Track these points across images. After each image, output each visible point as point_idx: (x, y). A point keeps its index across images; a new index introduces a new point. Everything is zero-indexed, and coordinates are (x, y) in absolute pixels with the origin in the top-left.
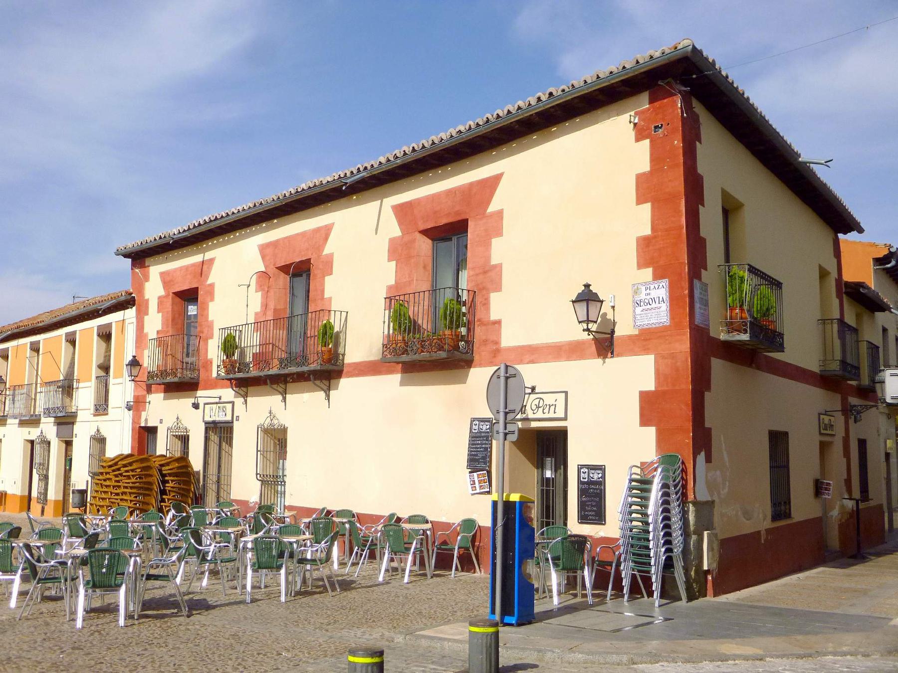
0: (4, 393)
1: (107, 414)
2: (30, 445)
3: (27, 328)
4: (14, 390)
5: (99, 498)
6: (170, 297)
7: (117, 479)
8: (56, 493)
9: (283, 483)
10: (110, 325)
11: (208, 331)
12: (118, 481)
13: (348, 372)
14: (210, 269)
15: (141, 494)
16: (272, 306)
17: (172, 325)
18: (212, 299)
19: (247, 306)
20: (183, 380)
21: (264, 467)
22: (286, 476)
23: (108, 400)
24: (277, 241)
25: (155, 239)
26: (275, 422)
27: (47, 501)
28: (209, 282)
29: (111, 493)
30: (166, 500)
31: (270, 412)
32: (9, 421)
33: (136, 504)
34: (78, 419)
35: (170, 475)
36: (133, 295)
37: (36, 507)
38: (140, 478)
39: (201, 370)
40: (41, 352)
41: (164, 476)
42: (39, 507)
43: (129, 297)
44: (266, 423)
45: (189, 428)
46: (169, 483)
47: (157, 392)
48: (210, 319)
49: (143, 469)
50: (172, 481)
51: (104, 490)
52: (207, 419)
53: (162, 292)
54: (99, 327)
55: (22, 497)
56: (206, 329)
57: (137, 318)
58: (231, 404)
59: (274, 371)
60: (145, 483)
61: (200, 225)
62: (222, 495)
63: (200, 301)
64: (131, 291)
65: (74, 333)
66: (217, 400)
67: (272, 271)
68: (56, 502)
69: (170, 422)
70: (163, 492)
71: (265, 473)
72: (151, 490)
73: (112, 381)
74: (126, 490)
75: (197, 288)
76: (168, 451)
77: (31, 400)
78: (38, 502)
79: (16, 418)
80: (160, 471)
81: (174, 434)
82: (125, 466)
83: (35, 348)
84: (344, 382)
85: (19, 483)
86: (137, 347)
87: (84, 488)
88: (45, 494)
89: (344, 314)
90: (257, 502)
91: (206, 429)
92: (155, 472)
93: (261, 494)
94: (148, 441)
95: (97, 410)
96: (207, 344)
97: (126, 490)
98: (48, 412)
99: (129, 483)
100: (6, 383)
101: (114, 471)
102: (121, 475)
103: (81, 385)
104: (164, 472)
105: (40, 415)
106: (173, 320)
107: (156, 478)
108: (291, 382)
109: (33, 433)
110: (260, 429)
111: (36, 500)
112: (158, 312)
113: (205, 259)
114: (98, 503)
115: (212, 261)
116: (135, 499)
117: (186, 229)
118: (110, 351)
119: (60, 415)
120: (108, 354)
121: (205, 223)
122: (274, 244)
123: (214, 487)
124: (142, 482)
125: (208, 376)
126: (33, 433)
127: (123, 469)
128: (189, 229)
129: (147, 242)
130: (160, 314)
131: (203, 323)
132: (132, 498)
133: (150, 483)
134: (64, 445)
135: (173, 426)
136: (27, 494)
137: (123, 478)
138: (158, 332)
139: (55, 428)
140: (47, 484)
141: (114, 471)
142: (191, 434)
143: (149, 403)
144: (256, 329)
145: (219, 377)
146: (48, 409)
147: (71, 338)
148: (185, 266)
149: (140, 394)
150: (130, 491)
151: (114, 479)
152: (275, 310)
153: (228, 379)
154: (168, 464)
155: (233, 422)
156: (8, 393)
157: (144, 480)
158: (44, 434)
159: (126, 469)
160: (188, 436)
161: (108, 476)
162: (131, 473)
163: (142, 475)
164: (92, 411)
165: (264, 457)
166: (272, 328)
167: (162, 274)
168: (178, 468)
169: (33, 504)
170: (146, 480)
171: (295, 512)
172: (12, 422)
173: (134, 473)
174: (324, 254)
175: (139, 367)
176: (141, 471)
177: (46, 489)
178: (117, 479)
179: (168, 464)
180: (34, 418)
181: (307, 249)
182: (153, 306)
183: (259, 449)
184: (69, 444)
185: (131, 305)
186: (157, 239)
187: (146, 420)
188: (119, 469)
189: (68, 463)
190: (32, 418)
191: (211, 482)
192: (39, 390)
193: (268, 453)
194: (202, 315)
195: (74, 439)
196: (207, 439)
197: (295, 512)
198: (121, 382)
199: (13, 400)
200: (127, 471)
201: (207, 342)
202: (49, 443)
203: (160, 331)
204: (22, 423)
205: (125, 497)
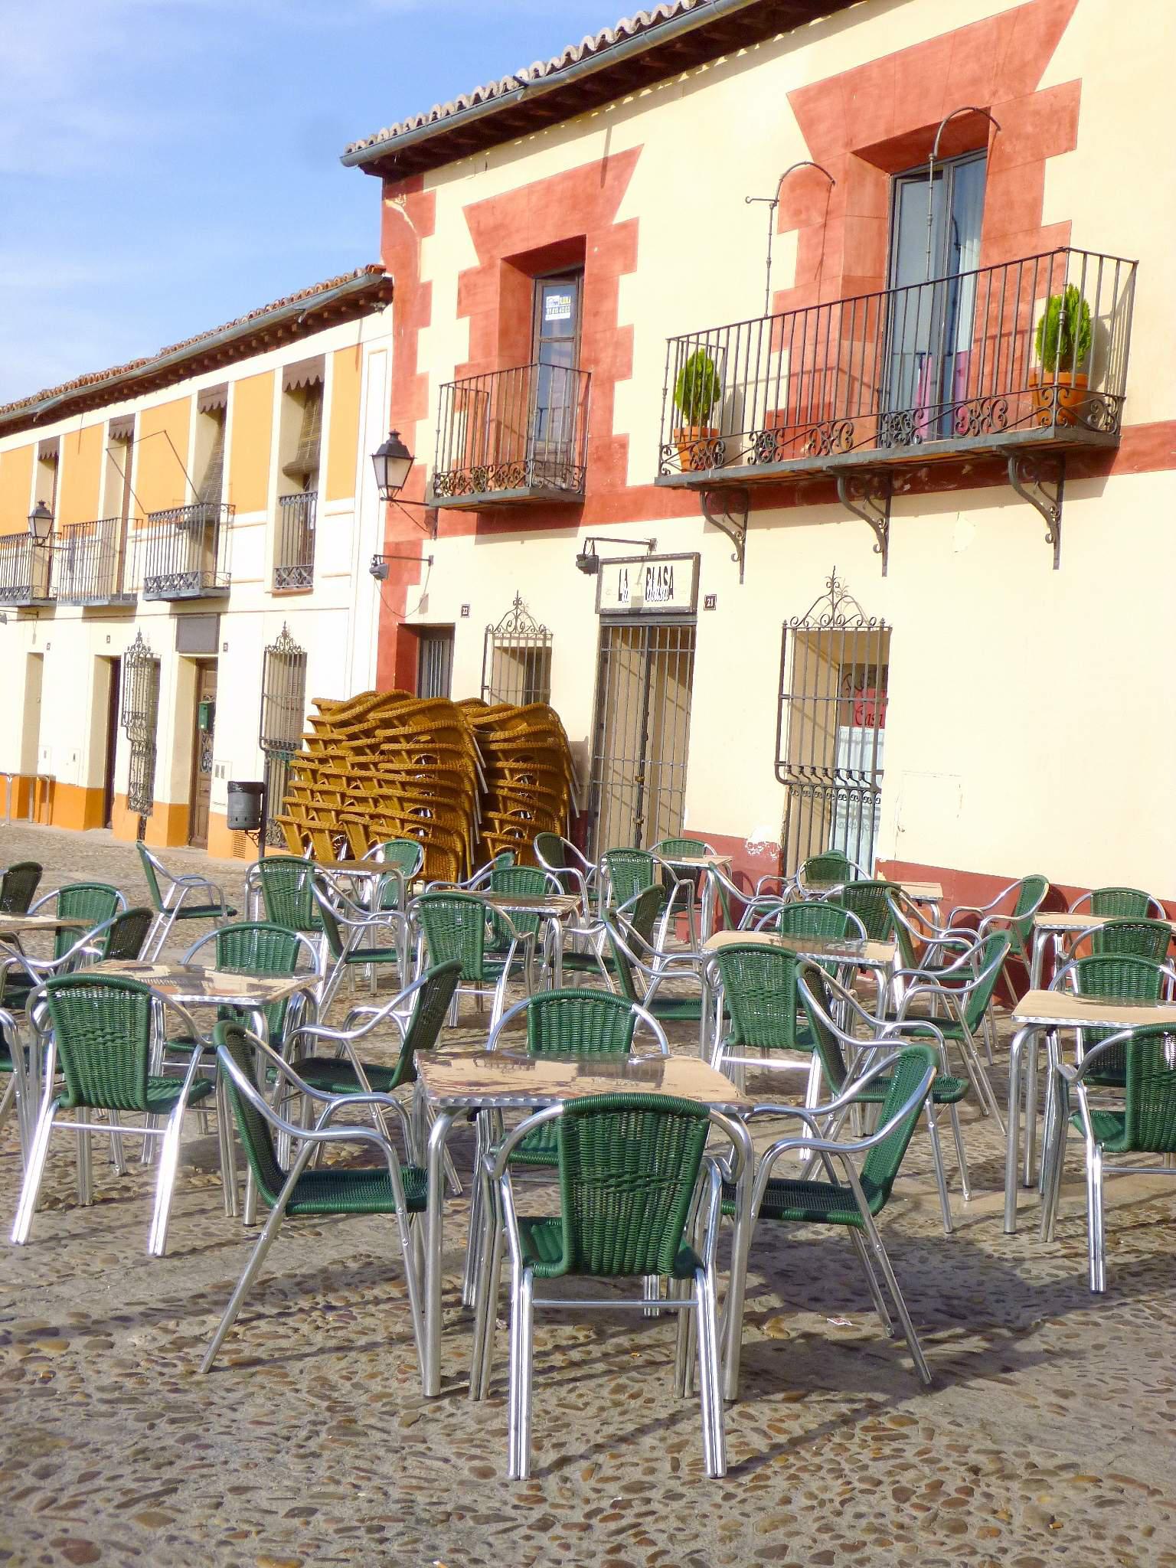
0: (47, 543)
1: (310, 592)
2: (109, 667)
3: (102, 384)
4: (73, 535)
5: (307, 809)
6: (497, 272)
7: (362, 759)
8: (175, 787)
9: (867, 794)
10: (318, 362)
11: (615, 357)
12: (364, 766)
13: (1134, 454)
14: (622, 180)
15: (430, 803)
16: (837, 265)
17: (501, 349)
18: (630, 266)
19: (769, 263)
20: (545, 494)
21: (796, 744)
22: (881, 772)
23: (311, 557)
24: (861, 73)
25: (461, 106)
26: (847, 611)
27: (151, 805)
28: (621, 216)
29: (343, 796)
30: (497, 823)
31: (832, 583)
32: (61, 611)
33: (415, 831)
34: (233, 604)
35: (507, 754)
36: (387, 275)
37: (124, 819)
38: (428, 759)
39: (591, 467)
40: (136, 437)
41: (490, 756)
42: (133, 818)
43: (376, 280)
44: (816, 613)
45: (550, 629)
46: (504, 777)
47: (452, 531)
48: (622, 321)
49: (438, 734)
50: (513, 771)
51: (318, 787)
52: (611, 603)
53: (471, 260)
54: (288, 370)
55: (91, 792)
56: (610, 351)
57: (397, 334)
58: (690, 563)
59: (866, 453)
60: (442, 773)
61: (603, 45)
62: (663, 823)
63: (590, 275)
64: (381, 263)
65: (222, 389)
66: (643, 551)
67: (840, 160)
68: (174, 809)
69: (492, 610)
70: (489, 802)
71: (806, 762)
72: (456, 793)
73: (323, 506)
74: (386, 791)
75: (580, 241)
76: (486, 692)
77: (115, 556)
78: (129, 807)
79: (76, 603)
80: (483, 742)
81: (506, 644)
82: (386, 724)
83: (123, 435)
84: (1118, 484)
85: (85, 760)
86: (396, 414)
87: (259, 778)
88: (148, 788)
89: (1126, 268)
90: (772, 845)
91: (604, 630)
92: (470, 746)
93: (787, 822)
94: (421, 658)
95: (280, 581)
96: (609, 393)
97: (386, 791)
98: (155, 587)
99: (397, 772)
100: (53, 519)
101: (352, 737)
102: (373, 748)
103: (239, 519)
104: (494, 747)
105: (135, 596)
106: (504, 333)
107: (470, 762)
108: (910, 492)
109: (118, 638)
110: (789, 632)
111: (124, 801)
112: (460, 314)
113: (612, 152)
114: (306, 823)
115: (629, 157)
116: (414, 817)
117: (558, 64)
118: (318, 430)
119: (186, 593)
120: (309, 439)
121: (623, 35)
122: (852, 83)
123: (629, 794)
124: (433, 772)
125: (613, 485)
126: (118, 638)
127: (381, 733)
128: (569, 61)
129: (435, 118)
130: (466, 321)
131: (598, 336)
132: (405, 815)
133: (455, 775)
134: (194, 668)
135: (504, 624)
136: (101, 784)
137: (376, 757)
138: (458, 369)
139: (173, 623)
140: (151, 765)
141: (352, 737)
142: (557, 646)
143: (430, 561)
144: (777, 341)
145: (664, 481)
146: (157, 579)
147: (215, 401)
148: (540, 182)
149: (401, 539)
150: (399, 793)
151: (352, 758)
152: (847, 281)
153: (693, 486)
154: (502, 724)
155: (694, 613)
156: (57, 543)
157: (439, 766)
158: (145, 642)
159: (390, 732)
160: (549, 651)
161: (332, 750)
162: (404, 745)
163: (434, 751)
164: (269, 583)
165: (804, 715)
166: (835, 334)
167: (473, 212)
168: (529, 736)
169: (118, 809)
170: (443, 767)
171: (730, 858)
172: (68, 613)
173: (411, 746)
174: (1042, 86)
175: (407, 463)
176: (432, 741)
177: (150, 775)
178: (362, 759)
179: (502, 724)
180: (120, 602)
181: (975, 81)
182: (444, 299)
183: (786, 691)
184: (205, 667)
185: (378, 300)
186: (467, 104)
187: (424, 601)
188: (368, 733)
189: (203, 717)
190: (117, 603)
191: (617, 779)
192: (131, 532)
193: (821, 704)
194: (596, 314)
195: (221, 656)
196: (604, 660)
197: (730, 858)
198: (349, 508)
199: (71, 563)
200: (393, 739)
201: (612, 389)
202: (156, 665)
203: (464, 366)
204: (93, 613)
205: (382, 809)
